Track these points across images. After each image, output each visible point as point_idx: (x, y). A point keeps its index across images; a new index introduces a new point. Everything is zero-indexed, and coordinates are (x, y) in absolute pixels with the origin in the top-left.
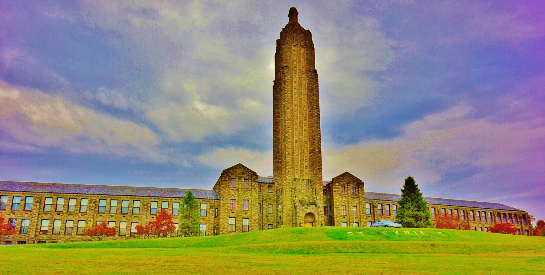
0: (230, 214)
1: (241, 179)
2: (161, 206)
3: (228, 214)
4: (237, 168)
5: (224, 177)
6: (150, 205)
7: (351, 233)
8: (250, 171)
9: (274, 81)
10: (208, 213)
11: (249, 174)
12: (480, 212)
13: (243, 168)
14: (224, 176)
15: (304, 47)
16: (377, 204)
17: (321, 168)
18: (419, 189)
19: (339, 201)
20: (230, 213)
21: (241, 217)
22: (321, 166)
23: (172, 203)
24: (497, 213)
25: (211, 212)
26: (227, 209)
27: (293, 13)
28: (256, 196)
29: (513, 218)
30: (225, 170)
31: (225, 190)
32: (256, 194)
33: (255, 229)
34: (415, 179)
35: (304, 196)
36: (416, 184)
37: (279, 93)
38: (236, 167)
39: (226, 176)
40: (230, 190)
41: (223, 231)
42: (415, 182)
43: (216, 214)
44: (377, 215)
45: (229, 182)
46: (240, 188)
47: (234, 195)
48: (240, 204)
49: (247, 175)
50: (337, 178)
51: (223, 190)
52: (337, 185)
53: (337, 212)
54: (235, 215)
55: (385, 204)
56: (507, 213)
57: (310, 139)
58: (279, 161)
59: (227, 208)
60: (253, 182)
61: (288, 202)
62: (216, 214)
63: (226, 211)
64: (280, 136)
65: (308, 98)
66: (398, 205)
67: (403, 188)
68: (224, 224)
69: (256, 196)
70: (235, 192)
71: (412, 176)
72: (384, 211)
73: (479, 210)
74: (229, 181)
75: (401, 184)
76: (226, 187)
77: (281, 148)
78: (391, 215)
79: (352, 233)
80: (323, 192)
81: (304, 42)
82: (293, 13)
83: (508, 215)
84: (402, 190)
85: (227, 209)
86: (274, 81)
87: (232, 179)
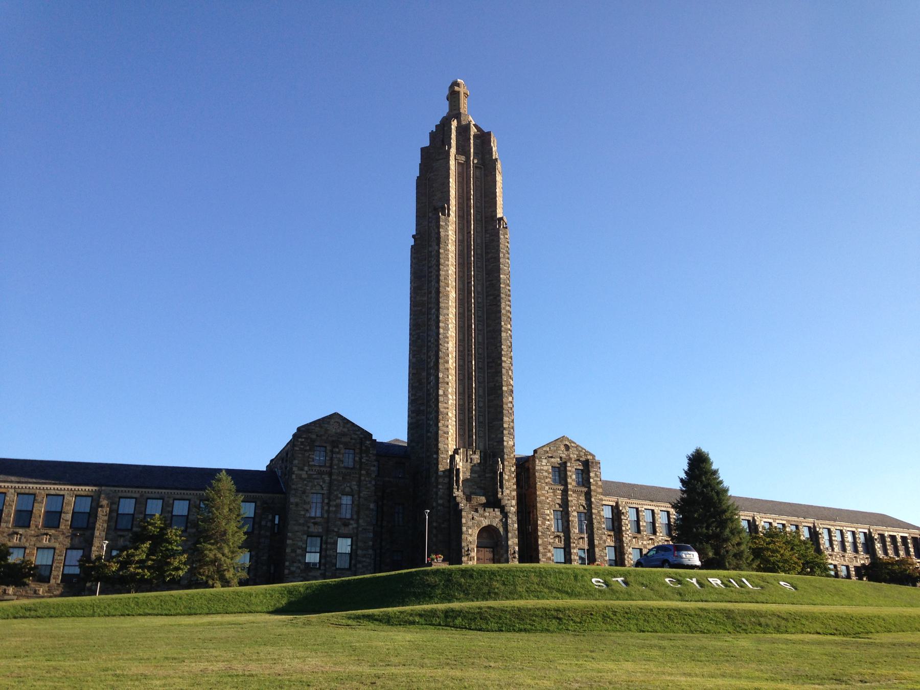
0: (309, 527)
1: (337, 447)
2: (143, 509)
3: (306, 528)
4: (329, 422)
5: (299, 443)
6: (116, 506)
7: (600, 582)
8: (358, 431)
9: (413, 236)
10: (256, 526)
11: (356, 436)
12: (844, 531)
13: (344, 423)
14: (300, 440)
15: (481, 168)
16: (627, 508)
17: (513, 428)
18: (720, 479)
19: (548, 501)
20: (311, 525)
21: (335, 534)
22: (512, 424)
23: (171, 502)
24: (878, 534)
25: (263, 523)
26: (304, 515)
27: (453, 96)
28: (369, 485)
29: (909, 541)
30: (303, 427)
31: (300, 472)
32: (370, 482)
33: (364, 561)
34: (712, 457)
35: (476, 487)
36: (714, 467)
37: (424, 262)
38: (328, 420)
39: (303, 440)
40: (312, 473)
41: (293, 569)
42: (712, 463)
43: (276, 527)
44: (628, 533)
45: (310, 453)
46: (335, 467)
47: (321, 484)
48: (335, 503)
49: (351, 439)
50: (544, 449)
51: (295, 472)
52: (543, 464)
53: (543, 524)
54: (320, 530)
55: (643, 509)
56: (897, 537)
57: (490, 365)
58: (422, 408)
59: (303, 513)
60: (365, 455)
61: (440, 502)
62: (276, 527)
63: (302, 521)
64: (424, 354)
65: (487, 276)
66: (672, 511)
67: (684, 476)
68: (294, 551)
69: (369, 485)
70: (323, 476)
71: (705, 449)
72: (641, 523)
73: (842, 528)
74: (310, 450)
75: (680, 468)
76: (304, 465)
77: (425, 380)
78: (658, 534)
79: (601, 581)
80: (515, 480)
81: (480, 156)
82: (453, 96)
83: (900, 540)
84: (682, 480)
85: (304, 515)
86: (413, 236)
87: (317, 446)
